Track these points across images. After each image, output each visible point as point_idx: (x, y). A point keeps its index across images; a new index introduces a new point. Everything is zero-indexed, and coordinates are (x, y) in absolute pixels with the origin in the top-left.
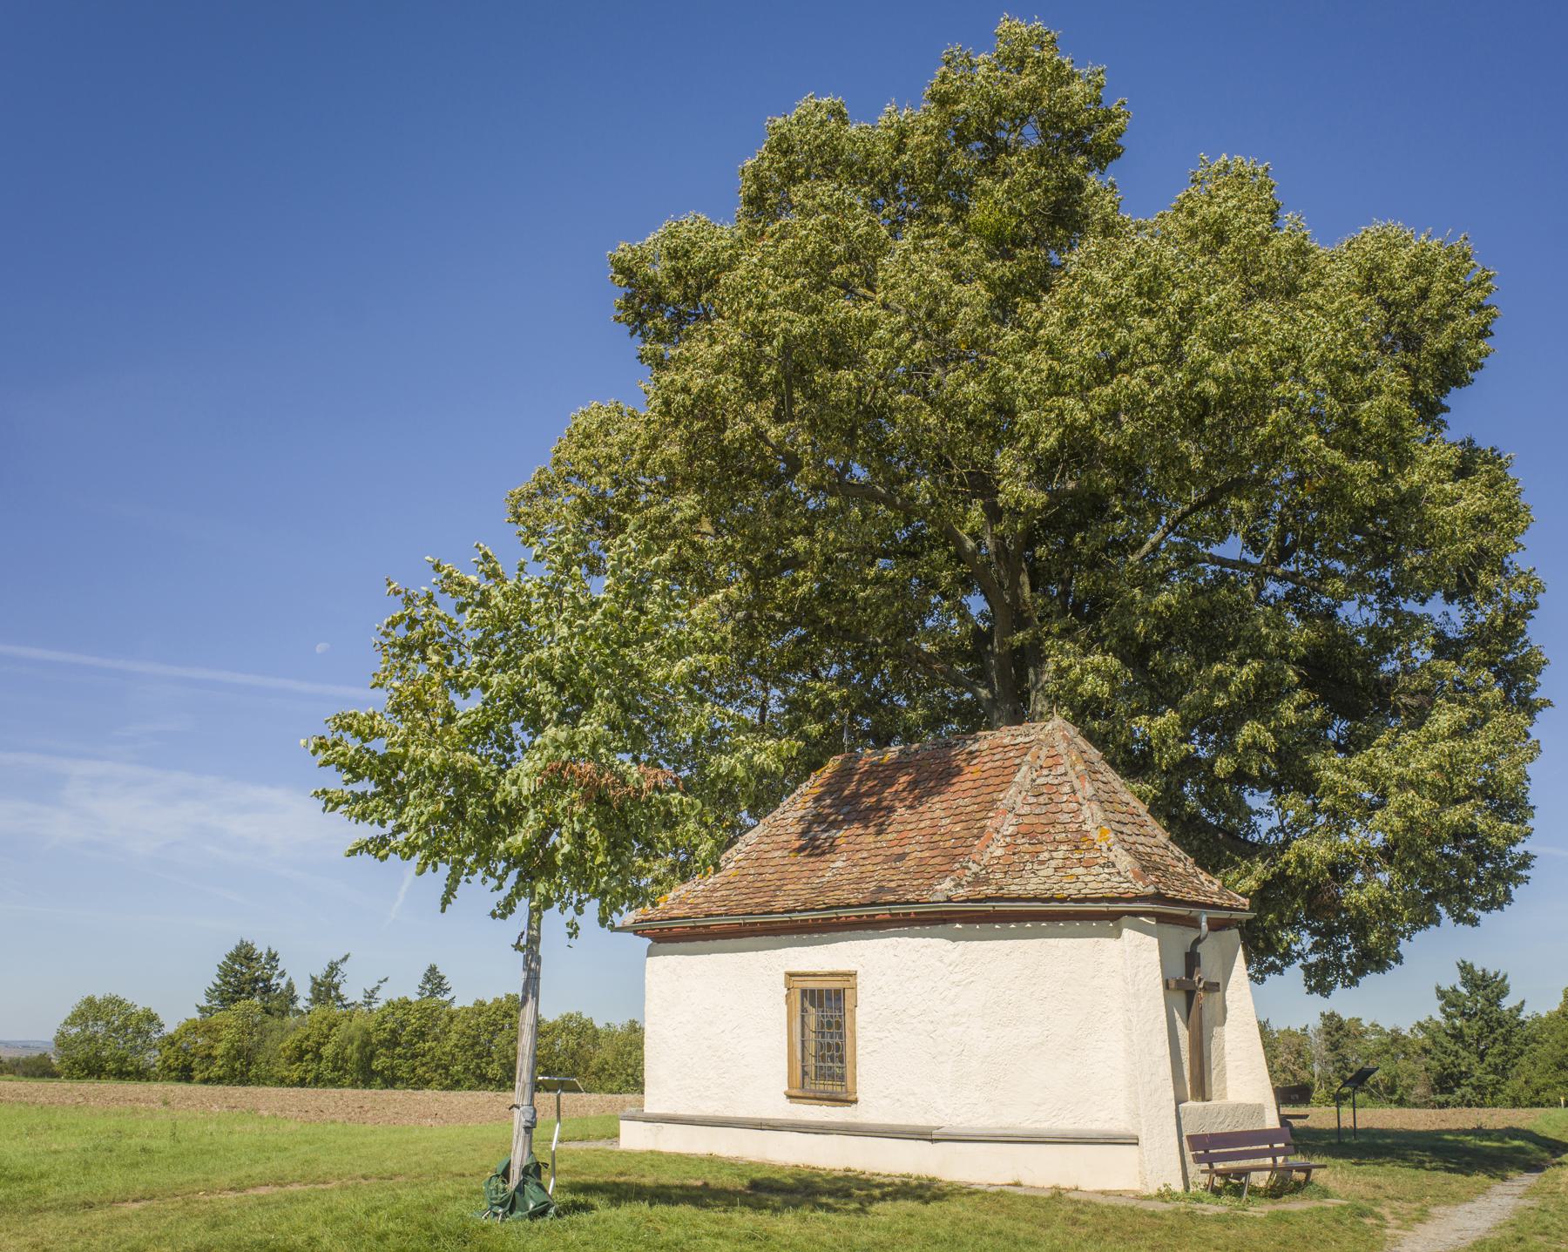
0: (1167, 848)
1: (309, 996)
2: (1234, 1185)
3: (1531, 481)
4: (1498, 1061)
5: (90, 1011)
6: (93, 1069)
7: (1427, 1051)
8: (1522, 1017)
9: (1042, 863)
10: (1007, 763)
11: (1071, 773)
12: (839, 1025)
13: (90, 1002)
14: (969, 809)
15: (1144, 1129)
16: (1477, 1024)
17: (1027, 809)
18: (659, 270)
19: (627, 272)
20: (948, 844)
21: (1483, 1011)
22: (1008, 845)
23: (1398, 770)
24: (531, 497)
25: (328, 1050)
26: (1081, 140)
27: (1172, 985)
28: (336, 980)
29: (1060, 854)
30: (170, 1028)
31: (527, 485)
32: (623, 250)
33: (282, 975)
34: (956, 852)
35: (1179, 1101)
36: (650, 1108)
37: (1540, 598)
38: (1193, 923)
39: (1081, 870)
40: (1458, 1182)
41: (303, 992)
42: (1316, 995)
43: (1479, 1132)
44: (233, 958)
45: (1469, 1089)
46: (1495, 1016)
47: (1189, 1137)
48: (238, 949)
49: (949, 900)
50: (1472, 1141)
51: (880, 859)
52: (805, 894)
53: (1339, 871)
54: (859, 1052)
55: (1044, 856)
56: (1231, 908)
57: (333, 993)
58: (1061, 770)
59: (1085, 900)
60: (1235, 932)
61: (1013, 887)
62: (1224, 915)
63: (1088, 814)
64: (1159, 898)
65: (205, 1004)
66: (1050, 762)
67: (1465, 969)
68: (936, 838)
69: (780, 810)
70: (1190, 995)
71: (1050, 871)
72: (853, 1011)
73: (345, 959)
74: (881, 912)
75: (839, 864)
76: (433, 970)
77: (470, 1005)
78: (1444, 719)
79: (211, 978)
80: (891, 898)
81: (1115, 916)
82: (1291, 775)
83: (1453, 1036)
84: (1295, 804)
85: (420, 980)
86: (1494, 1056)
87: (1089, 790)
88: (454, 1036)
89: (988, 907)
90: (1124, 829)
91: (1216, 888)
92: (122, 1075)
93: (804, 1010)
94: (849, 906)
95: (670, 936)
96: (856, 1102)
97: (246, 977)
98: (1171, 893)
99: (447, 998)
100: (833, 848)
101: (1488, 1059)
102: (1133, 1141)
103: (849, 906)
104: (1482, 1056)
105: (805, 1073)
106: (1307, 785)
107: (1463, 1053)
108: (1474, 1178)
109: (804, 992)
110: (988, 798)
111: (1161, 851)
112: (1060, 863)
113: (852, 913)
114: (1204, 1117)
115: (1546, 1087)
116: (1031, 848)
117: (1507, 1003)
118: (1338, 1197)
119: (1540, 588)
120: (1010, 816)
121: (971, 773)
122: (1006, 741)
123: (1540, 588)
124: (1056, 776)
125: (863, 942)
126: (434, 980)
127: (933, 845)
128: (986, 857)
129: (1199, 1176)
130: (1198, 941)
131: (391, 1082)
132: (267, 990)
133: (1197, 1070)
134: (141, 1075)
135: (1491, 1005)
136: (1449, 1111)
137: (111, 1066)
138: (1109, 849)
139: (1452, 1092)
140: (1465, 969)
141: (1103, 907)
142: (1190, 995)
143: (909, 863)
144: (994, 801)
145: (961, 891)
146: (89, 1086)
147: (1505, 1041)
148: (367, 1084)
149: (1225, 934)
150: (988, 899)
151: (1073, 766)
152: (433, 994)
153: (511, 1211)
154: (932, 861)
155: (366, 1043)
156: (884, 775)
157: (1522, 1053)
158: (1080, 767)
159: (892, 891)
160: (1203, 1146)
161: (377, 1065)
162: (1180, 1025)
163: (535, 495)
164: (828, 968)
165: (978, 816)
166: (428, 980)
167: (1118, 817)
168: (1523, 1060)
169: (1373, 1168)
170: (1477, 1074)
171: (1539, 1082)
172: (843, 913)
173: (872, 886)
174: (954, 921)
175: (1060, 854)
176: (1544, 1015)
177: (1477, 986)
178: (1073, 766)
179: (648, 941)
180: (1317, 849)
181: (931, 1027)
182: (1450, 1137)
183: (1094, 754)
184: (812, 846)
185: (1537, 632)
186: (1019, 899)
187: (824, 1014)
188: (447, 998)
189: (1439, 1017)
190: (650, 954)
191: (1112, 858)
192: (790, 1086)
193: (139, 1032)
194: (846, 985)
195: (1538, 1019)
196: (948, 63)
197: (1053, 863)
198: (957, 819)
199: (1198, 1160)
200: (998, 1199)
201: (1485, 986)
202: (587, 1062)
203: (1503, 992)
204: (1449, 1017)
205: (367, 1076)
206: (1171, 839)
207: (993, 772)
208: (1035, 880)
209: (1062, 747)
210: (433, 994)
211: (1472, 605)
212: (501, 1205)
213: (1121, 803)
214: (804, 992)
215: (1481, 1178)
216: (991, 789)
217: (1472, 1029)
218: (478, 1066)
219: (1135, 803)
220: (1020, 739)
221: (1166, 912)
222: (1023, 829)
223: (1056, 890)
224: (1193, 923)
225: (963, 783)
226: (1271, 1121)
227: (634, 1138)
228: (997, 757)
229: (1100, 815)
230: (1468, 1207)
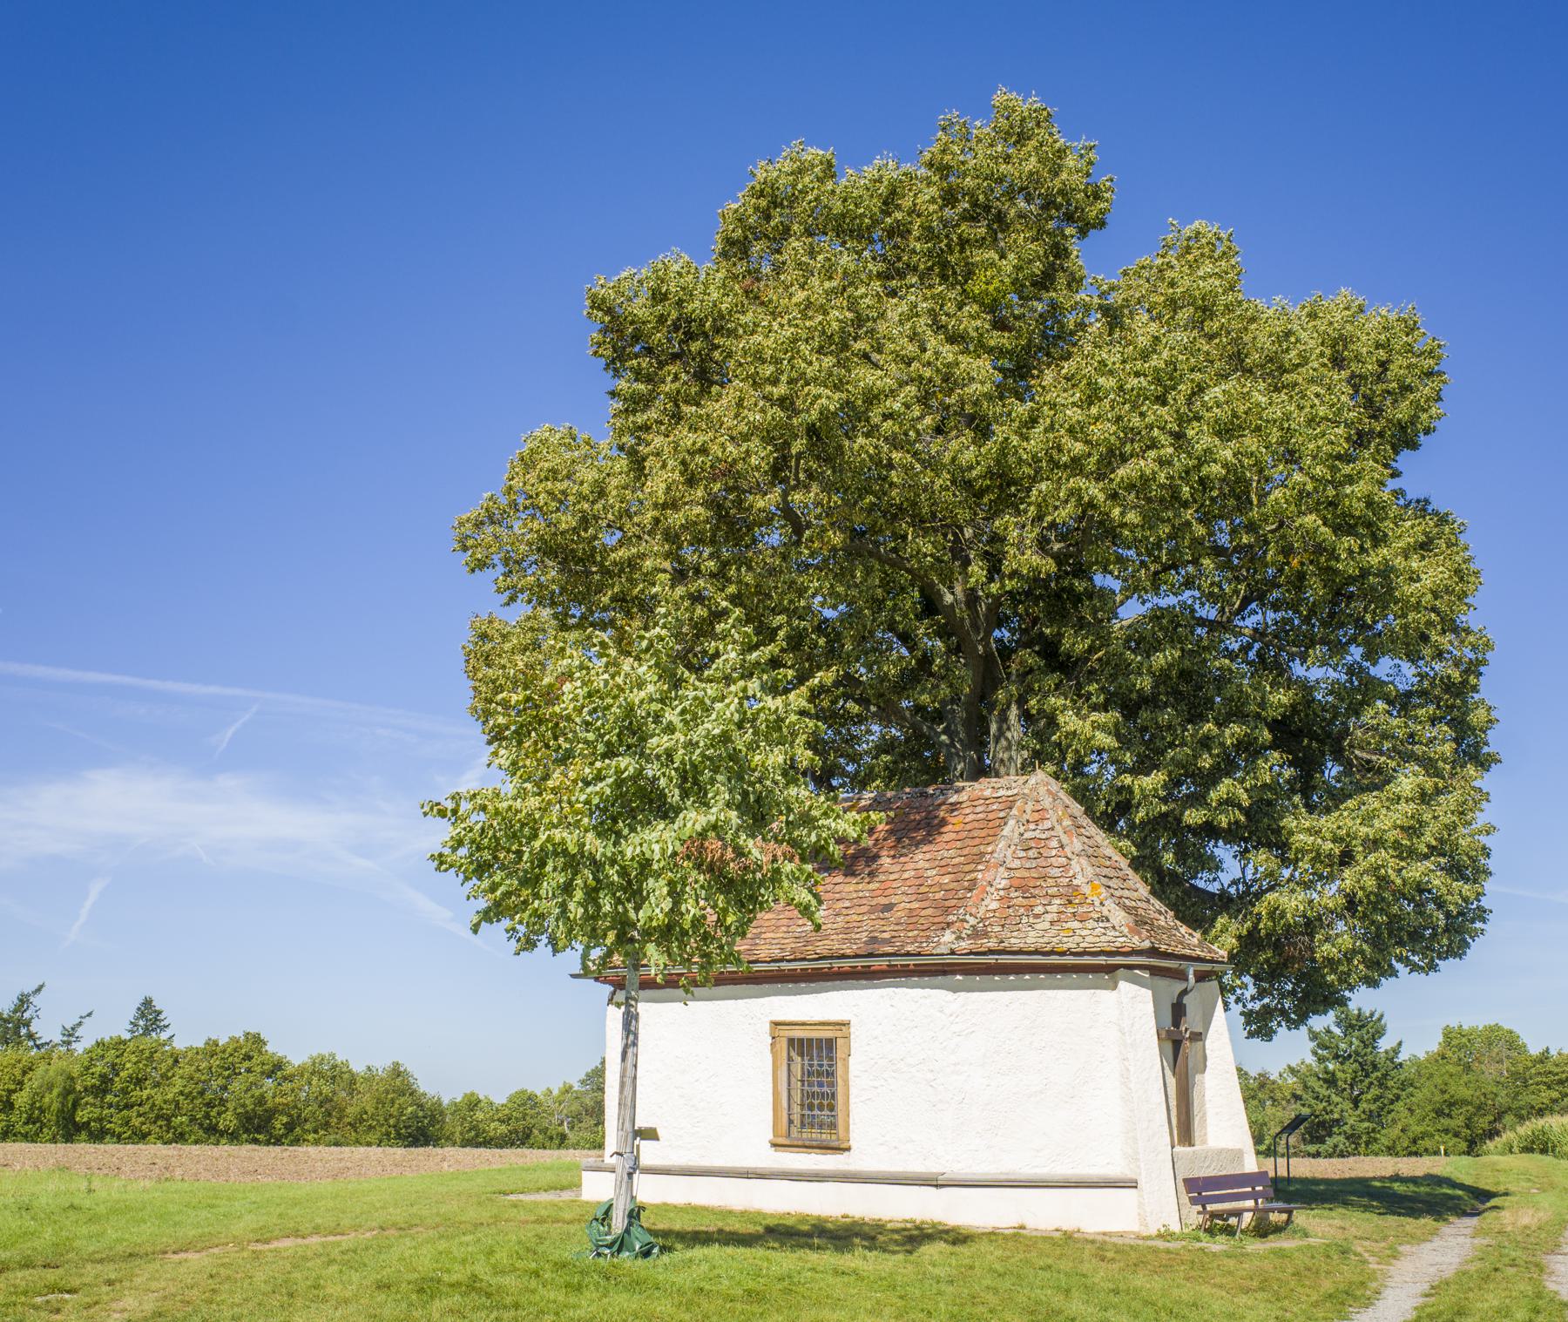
2: (1219, 1226)
3: (1479, 545)
4: (1373, 1107)
7: (1297, 1097)
8: (1402, 1058)
10: (991, 816)
11: (1058, 828)
12: (830, 1074)
14: (955, 861)
16: (1351, 1066)
17: (1017, 864)
18: (640, 308)
19: (598, 304)
20: (938, 896)
23: (1364, 830)
24: (479, 525)
25: (21, 1099)
26: (1069, 213)
28: (26, 1015)
29: (1054, 908)
31: (474, 512)
32: (603, 286)
34: (947, 904)
37: (1489, 655)
38: (1182, 976)
39: (1076, 925)
40: (1410, 1224)
42: (1256, 1041)
43: (1396, 1178)
45: (1342, 1138)
46: (1370, 1058)
47: (1185, 1181)
49: (953, 952)
50: (1398, 1187)
51: (864, 909)
53: (1311, 925)
54: (852, 1100)
55: (1039, 910)
56: (1212, 961)
57: (23, 1031)
58: (1047, 824)
59: (1084, 953)
61: (1013, 941)
62: (1207, 967)
63: (1078, 869)
64: (1153, 952)
66: (1036, 816)
68: (923, 889)
70: (1177, 1045)
71: (1047, 925)
72: (846, 1061)
73: (39, 990)
74: (879, 964)
76: (148, 1003)
77: (201, 1045)
78: (1408, 781)
80: (889, 949)
81: (1111, 969)
82: (1259, 827)
83: (1325, 1081)
84: (1262, 859)
85: (131, 1013)
86: (1368, 1101)
87: (1077, 845)
88: (179, 1083)
89: (991, 959)
90: (1110, 883)
91: (1195, 941)
93: (790, 1059)
94: (844, 956)
96: (848, 1149)
98: (1163, 947)
99: (164, 1036)
101: (1363, 1105)
102: (1132, 1185)
103: (844, 956)
104: (1356, 1102)
105: (791, 1122)
106: (1279, 844)
107: (1335, 1099)
108: (1422, 1221)
109: (791, 1041)
110: (975, 850)
111: (1144, 905)
113: (846, 964)
115: (1424, 1135)
116: (1025, 902)
117: (1384, 1044)
118: (1316, 1236)
119: (1488, 646)
120: (1002, 869)
121: (956, 822)
122: (988, 793)
123: (1488, 646)
124: (1044, 831)
125: (855, 992)
126: (149, 1016)
127: (922, 897)
128: (982, 910)
129: (1194, 1216)
130: (1185, 992)
131: (98, 1136)
133: (1183, 1117)
135: (1366, 1046)
136: (1320, 1160)
139: (1323, 1142)
141: (1101, 960)
142: (1177, 1045)
143: (899, 914)
144: (982, 854)
145: (963, 944)
147: (1381, 1085)
148: (69, 1138)
150: (991, 952)
151: (1059, 821)
152: (147, 1032)
153: (619, 1251)
154: (923, 913)
155: (67, 1092)
157: (1398, 1098)
158: (1067, 822)
159: (888, 942)
160: (1198, 1188)
161: (82, 1116)
162: (1168, 1073)
163: (482, 523)
165: (967, 868)
166: (143, 1015)
167: (1105, 871)
168: (1399, 1106)
169: (1326, 1213)
170: (1351, 1121)
171: (1417, 1129)
172: (837, 964)
173: (864, 936)
174: (954, 973)
175: (1054, 908)
176: (1422, 1056)
177: (1351, 1026)
178: (1059, 821)
179: (609, 988)
180: (1292, 903)
182: (1378, 1184)
183: (1077, 809)
185: (1489, 689)
186: (1020, 952)
187: (813, 1065)
188: (164, 1036)
189: (1311, 1060)
191: (1105, 913)
194: (838, 1034)
196: (944, 129)
197: (1048, 917)
198: (943, 870)
199: (1193, 1201)
200: (1017, 1238)
202: (342, 1110)
203: (1379, 1033)
204: (1321, 1060)
205: (70, 1129)
207: (976, 825)
208: (1032, 934)
209: (1047, 802)
210: (147, 1032)
211: (1421, 663)
212: (609, 1246)
214: (791, 1041)
215: (1427, 1222)
216: (977, 841)
217: (1345, 1072)
218: (207, 1116)
219: (1117, 857)
220: (1001, 793)
221: (1158, 965)
222: (1016, 883)
224: (1180, 975)
225: (948, 834)
226: (1251, 1164)
228: (979, 809)
229: (1090, 871)
230: (1428, 1245)
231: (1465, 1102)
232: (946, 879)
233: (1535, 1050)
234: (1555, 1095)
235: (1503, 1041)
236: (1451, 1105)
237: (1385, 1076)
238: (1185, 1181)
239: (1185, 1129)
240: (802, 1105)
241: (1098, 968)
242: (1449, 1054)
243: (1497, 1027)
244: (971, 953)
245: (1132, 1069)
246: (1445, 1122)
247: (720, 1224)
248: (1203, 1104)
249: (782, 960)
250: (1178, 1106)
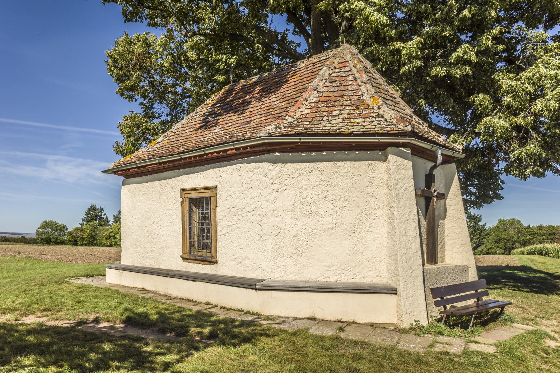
0: (411, 117)
1: (113, 220)
5: (45, 225)
6: (48, 241)
8: (485, 227)
9: (335, 116)
11: (354, 70)
13: (45, 222)
15: (402, 285)
17: (326, 89)
21: (473, 226)
22: (312, 108)
27: (419, 193)
29: (347, 112)
30: (70, 230)
35: (423, 265)
36: (125, 261)
43: (508, 267)
44: (90, 210)
47: (432, 290)
48: (91, 207)
58: (347, 69)
59: (364, 135)
60: (454, 165)
63: (365, 90)
65: (82, 223)
66: (341, 65)
69: (195, 112)
70: (428, 200)
71: (340, 121)
72: (215, 210)
79: (83, 215)
81: (383, 147)
93: (190, 210)
96: (216, 262)
100: (217, 124)
101: (474, 240)
102: (393, 291)
105: (191, 245)
109: (190, 199)
112: (346, 116)
116: (327, 109)
117: (480, 224)
120: (315, 92)
124: (345, 72)
130: (435, 167)
132: (100, 219)
133: (431, 246)
134: (62, 243)
137: (53, 240)
138: (379, 108)
141: (375, 140)
142: (428, 200)
146: (46, 247)
147: (480, 235)
151: (355, 67)
156: (247, 90)
160: (439, 294)
162: (422, 218)
164: (202, 185)
165: (295, 96)
168: (485, 240)
174: (274, 151)
176: (491, 227)
179: (122, 178)
181: (259, 218)
184: (206, 125)
186: (317, 135)
187: (200, 210)
190: (123, 184)
191: (381, 112)
192: (184, 252)
193: (61, 231)
195: (489, 228)
197: (342, 117)
206: (413, 112)
207: (306, 76)
209: (348, 58)
213: (385, 90)
214: (190, 199)
222: (323, 99)
223: (344, 130)
224: (431, 157)
231: (504, 239)
232: (283, 104)
233: (525, 225)
234: (531, 237)
235: (514, 223)
236: (500, 240)
237: (481, 232)
238: (432, 290)
239: (431, 252)
240: (199, 236)
242: (500, 226)
243: (514, 219)
244: (283, 135)
245: (396, 213)
246: (498, 244)
248: (443, 238)
250: (428, 239)
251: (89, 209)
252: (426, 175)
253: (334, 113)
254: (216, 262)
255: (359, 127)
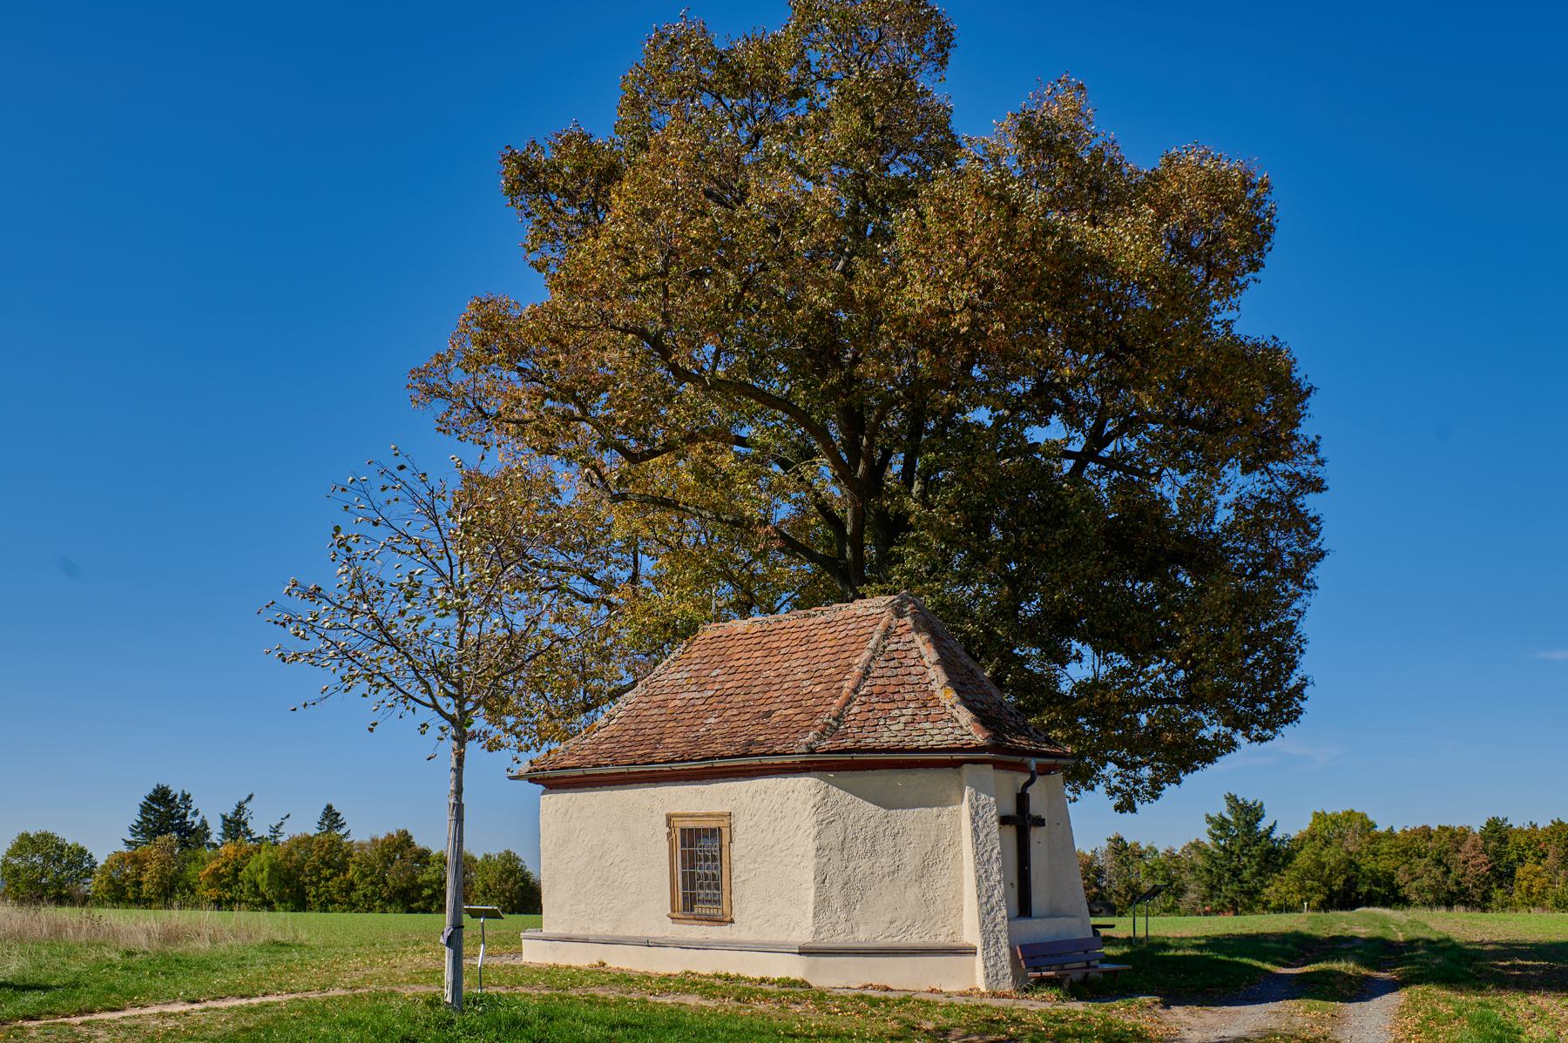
1: (221, 830)
5: (26, 844)
8: (1274, 836)
29: (910, 711)
33: (196, 813)
41: (216, 832)
48: (156, 791)
49: (812, 751)
51: (747, 716)
52: (682, 748)
67: (1232, 799)
71: (901, 726)
73: (250, 797)
75: (712, 720)
76: (329, 808)
79: (134, 816)
80: (762, 750)
81: (957, 764)
85: (318, 816)
92: (60, 900)
94: (722, 757)
95: (555, 781)
96: (732, 921)
97: (163, 813)
99: (342, 832)
103: (722, 757)
109: (683, 830)
114: (1039, 929)
117: (1263, 825)
122: (859, 613)
126: (331, 817)
140: (1232, 799)
143: (775, 719)
149: (1050, 777)
152: (330, 828)
159: (762, 744)
179: (541, 788)
186: (873, 750)
188: (342, 832)
189: (1207, 840)
192: (673, 911)
197: (903, 719)
201: (1250, 814)
210: (330, 828)
214: (683, 830)
224: (1022, 768)
227: (535, 953)
232: (818, 688)
241: (949, 761)
247: (1450, 914)
249: (673, 761)
251: (151, 798)
252: (1018, 796)
253: (894, 713)
254: (732, 921)
255: (927, 738)
